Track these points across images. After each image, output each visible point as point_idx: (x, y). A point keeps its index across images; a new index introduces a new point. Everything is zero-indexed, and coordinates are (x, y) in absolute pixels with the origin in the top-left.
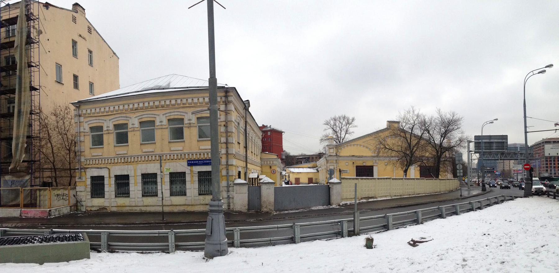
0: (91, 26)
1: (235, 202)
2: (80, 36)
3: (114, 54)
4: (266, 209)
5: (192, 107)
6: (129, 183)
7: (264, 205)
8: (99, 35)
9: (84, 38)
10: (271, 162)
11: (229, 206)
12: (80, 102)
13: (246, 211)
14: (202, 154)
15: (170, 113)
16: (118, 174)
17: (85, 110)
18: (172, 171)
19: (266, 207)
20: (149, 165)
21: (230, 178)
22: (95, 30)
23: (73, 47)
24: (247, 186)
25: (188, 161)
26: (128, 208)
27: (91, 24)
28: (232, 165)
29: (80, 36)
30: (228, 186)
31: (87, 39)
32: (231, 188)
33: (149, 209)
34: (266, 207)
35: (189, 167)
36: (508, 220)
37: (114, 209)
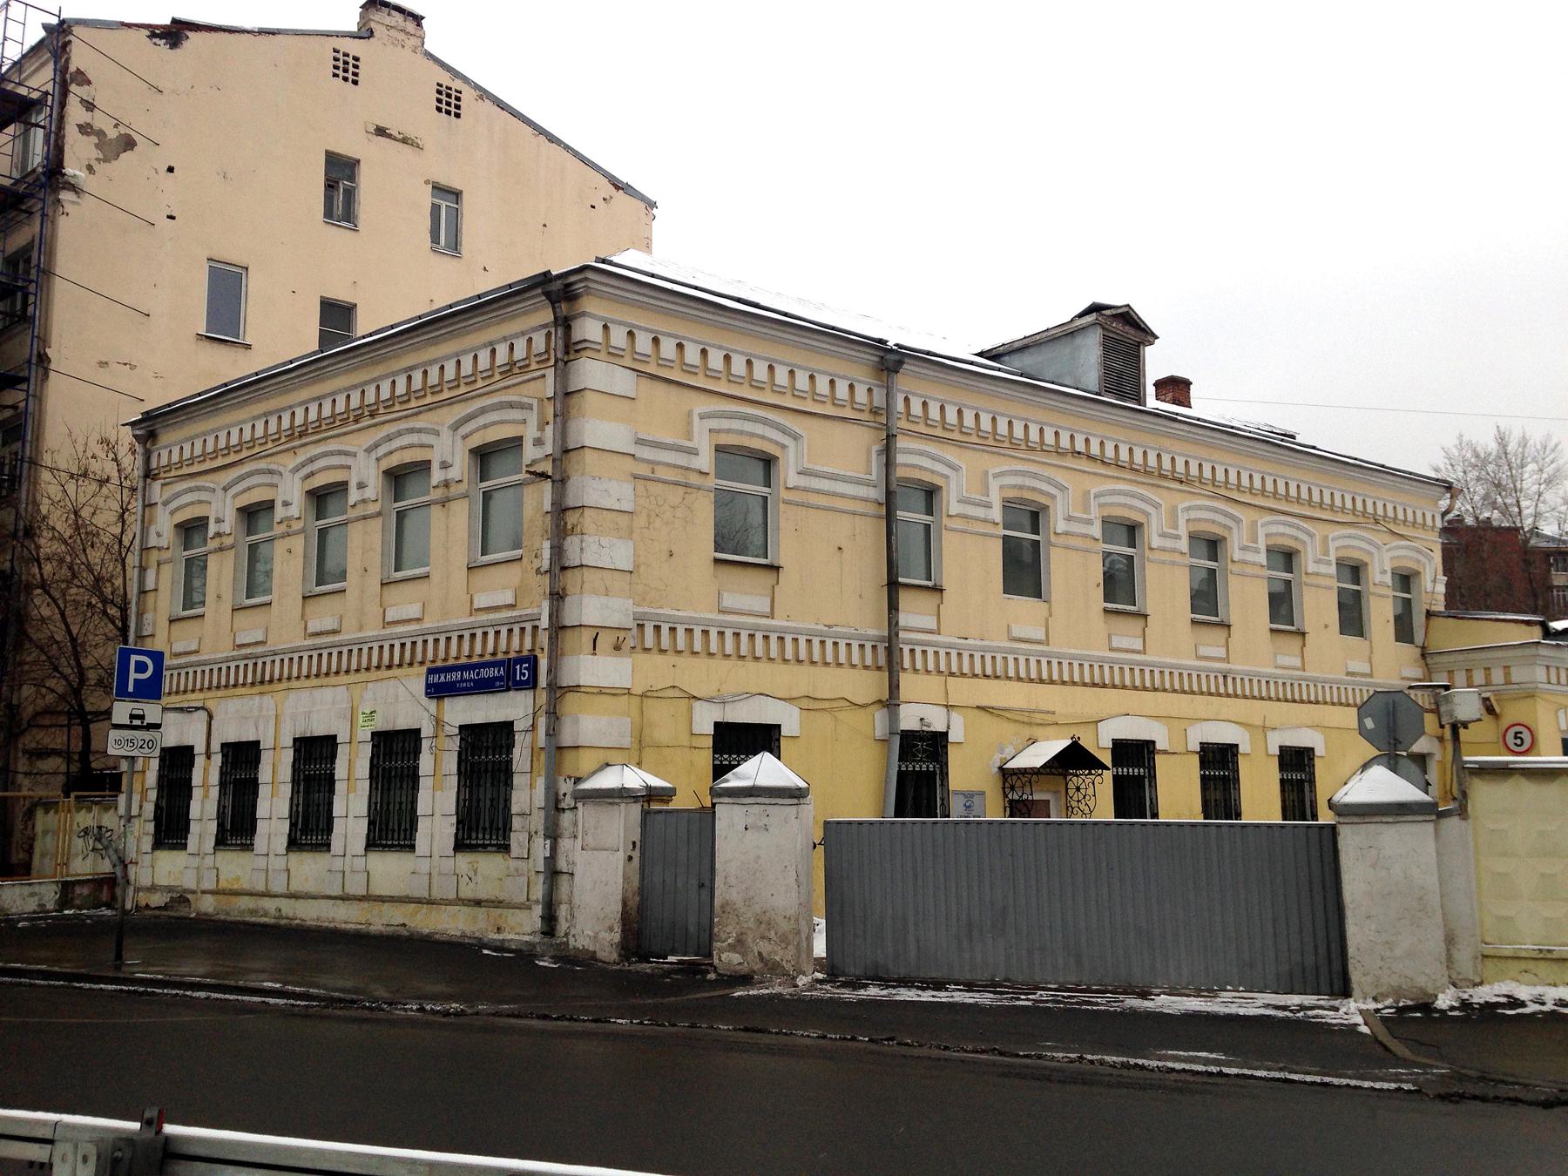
0: (457, 84)
1: (576, 901)
2: (381, 132)
3: (618, 185)
4: (736, 958)
5: (451, 402)
6: (256, 779)
7: (727, 932)
8: (515, 114)
9: (405, 141)
10: (1498, 676)
11: (550, 919)
12: (149, 417)
13: (615, 956)
14: (729, 633)
15: (389, 438)
16: (232, 739)
17: (173, 446)
18: (381, 725)
19: (739, 945)
20: (318, 693)
21: (571, 763)
22: (484, 94)
23: (330, 186)
24: (636, 810)
25: (431, 671)
26: (245, 903)
27: (456, 74)
28: (576, 688)
29: (381, 132)
30: (555, 806)
31: (427, 142)
32: (566, 819)
33: (309, 913)
34: (739, 945)
35: (432, 705)
36: (36, 1168)
37: (207, 905)
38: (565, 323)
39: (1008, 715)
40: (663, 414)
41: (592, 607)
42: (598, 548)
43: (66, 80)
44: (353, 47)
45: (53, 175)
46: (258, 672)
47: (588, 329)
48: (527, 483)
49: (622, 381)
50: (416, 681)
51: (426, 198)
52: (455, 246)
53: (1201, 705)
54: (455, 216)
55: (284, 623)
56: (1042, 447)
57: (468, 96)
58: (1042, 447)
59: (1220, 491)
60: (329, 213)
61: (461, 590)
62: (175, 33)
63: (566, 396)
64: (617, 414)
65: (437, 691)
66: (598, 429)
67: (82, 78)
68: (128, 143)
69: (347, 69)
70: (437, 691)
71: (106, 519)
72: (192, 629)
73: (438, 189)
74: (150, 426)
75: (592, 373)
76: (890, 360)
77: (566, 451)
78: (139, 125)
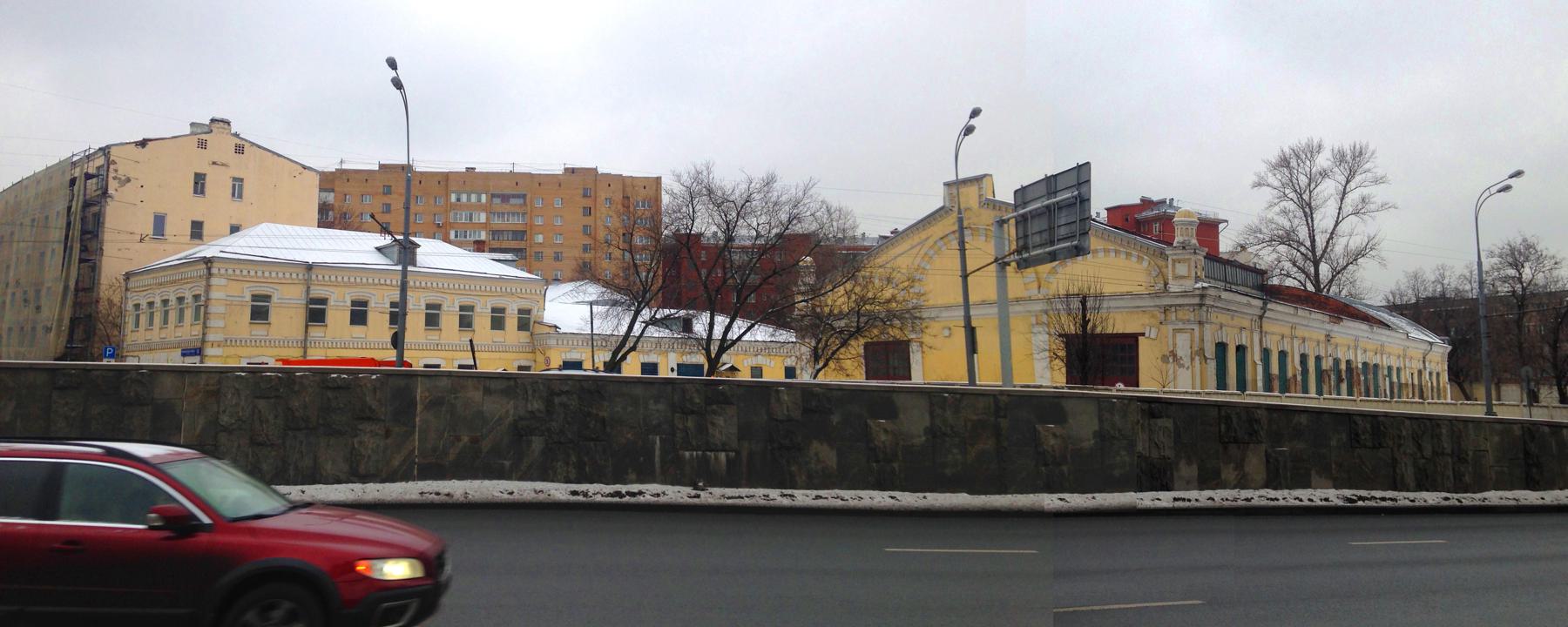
3: (305, 167)
22: (253, 144)
38: (209, 269)
39: (628, 346)
40: (235, 289)
41: (211, 337)
42: (212, 323)
43: (109, 163)
44: (204, 137)
45: (105, 193)
46: (150, 348)
47: (214, 271)
48: (202, 308)
49: (223, 282)
50: (179, 351)
51: (230, 183)
52: (240, 196)
53: (426, 353)
54: (241, 187)
55: (155, 335)
56: (362, 284)
57: (247, 145)
58: (362, 284)
59: (438, 290)
60: (195, 192)
61: (189, 331)
62: (143, 143)
63: (208, 286)
64: (220, 290)
65: (184, 355)
66: (214, 294)
67: (114, 162)
68: (128, 180)
69: (203, 145)
70: (184, 355)
71: (116, 300)
72: (134, 336)
73: (235, 179)
74: (128, 276)
75: (214, 281)
76: (309, 267)
77: (208, 299)
78: (131, 175)
